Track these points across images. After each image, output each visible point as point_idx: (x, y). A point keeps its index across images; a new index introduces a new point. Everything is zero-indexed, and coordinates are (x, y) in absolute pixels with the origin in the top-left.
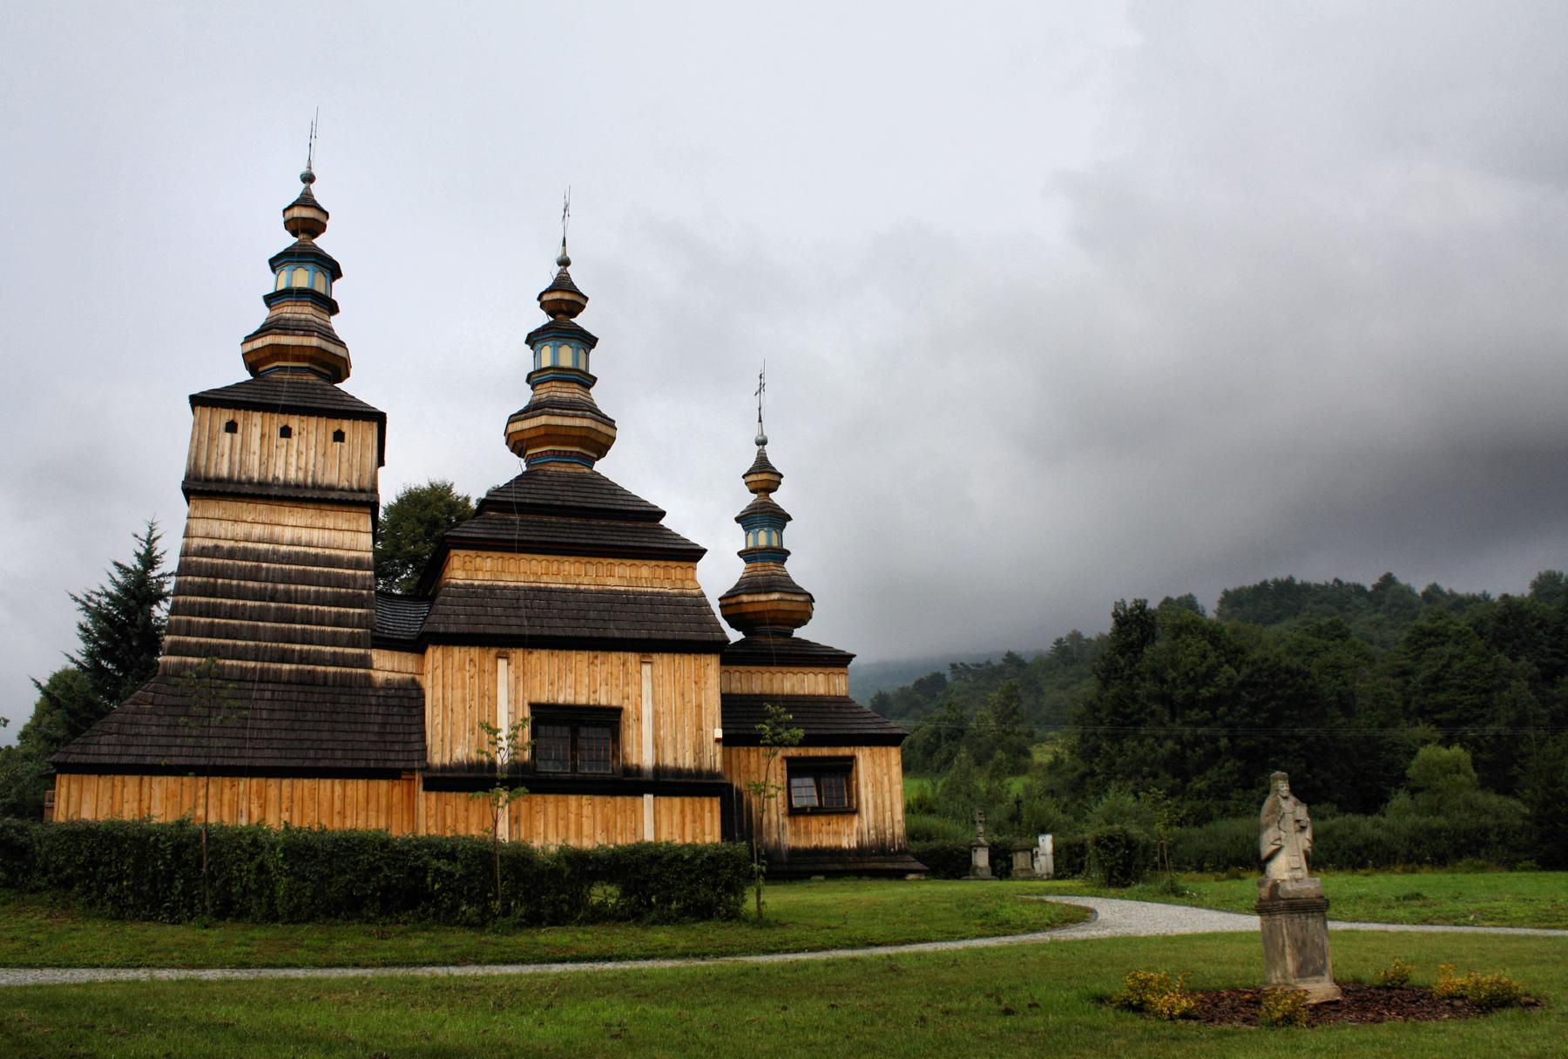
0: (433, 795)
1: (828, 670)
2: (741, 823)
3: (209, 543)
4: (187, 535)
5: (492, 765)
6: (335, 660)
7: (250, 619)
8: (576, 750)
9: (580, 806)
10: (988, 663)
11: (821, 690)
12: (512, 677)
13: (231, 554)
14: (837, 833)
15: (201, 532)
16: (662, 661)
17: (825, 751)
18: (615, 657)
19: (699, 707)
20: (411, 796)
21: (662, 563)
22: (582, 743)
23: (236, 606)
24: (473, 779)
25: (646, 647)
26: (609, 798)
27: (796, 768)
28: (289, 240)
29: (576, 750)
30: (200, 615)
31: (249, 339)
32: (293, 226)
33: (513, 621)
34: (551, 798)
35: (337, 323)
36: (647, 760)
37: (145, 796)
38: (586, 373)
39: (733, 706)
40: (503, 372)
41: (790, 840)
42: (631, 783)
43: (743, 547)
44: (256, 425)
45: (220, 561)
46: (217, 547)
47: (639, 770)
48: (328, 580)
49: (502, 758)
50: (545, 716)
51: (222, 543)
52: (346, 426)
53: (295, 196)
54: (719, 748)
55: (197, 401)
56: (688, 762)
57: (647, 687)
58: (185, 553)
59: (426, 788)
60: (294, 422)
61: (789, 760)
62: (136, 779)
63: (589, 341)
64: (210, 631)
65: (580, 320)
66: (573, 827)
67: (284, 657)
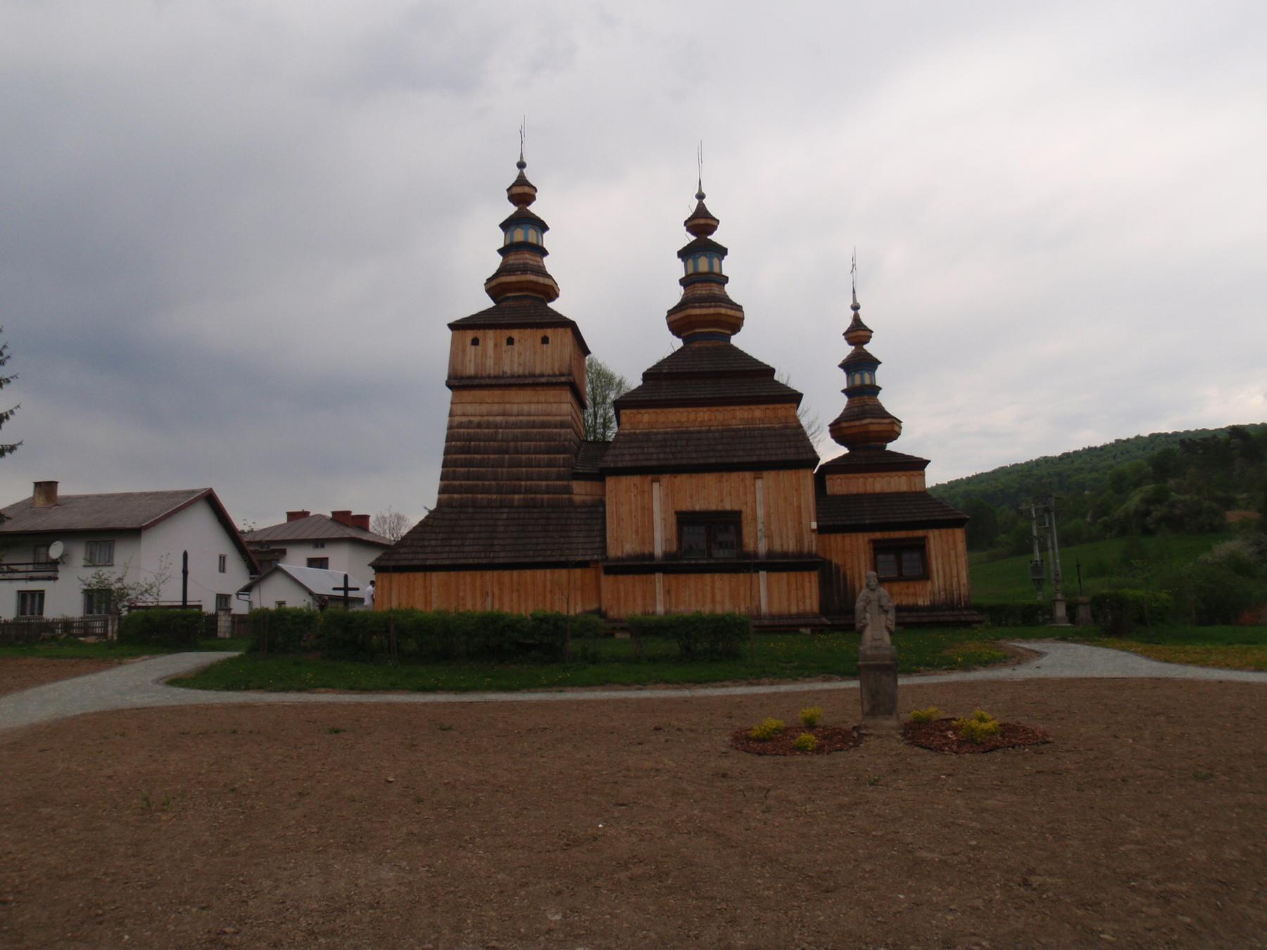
0: (611, 578)
1: (909, 473)
3: (464, 419)
4: (451, 415)
5: (652, 556)
8: (711, 542)
9: (713, 582)
11: (904, 488)
13: (479, 426)
15: (459, 412)
16: (769, 476)
17: (903, 534)
18: (735, 476)
19: (799, 507)
21: (771, 406)
24: (641, 566)
25: (758, 467)
26: (734, 575)
27: (879, 548)
29: (711, 542)
32: (513, 198)
33: (662, 456)
34: (693, 576)
35: (547, 261)
36: (762, 548)
38: (720, 275)
42: (747, 564)
43: (845, 387)
44: (490, 338)
46: (470, 422)
47: (755, 555)
49: (658, 551)
50: (685, 520)
51: (472, 419)
52: (549, 332)
54: (814, 536)
55: (453, 326)
56: (791, 546)
57: (759, 496)
60: (515, 334)
61: (874, 542)
63: (722, 252)
64: (468, 477)
65: (715, 237)
66: (709, 596)
67: (516, 491)
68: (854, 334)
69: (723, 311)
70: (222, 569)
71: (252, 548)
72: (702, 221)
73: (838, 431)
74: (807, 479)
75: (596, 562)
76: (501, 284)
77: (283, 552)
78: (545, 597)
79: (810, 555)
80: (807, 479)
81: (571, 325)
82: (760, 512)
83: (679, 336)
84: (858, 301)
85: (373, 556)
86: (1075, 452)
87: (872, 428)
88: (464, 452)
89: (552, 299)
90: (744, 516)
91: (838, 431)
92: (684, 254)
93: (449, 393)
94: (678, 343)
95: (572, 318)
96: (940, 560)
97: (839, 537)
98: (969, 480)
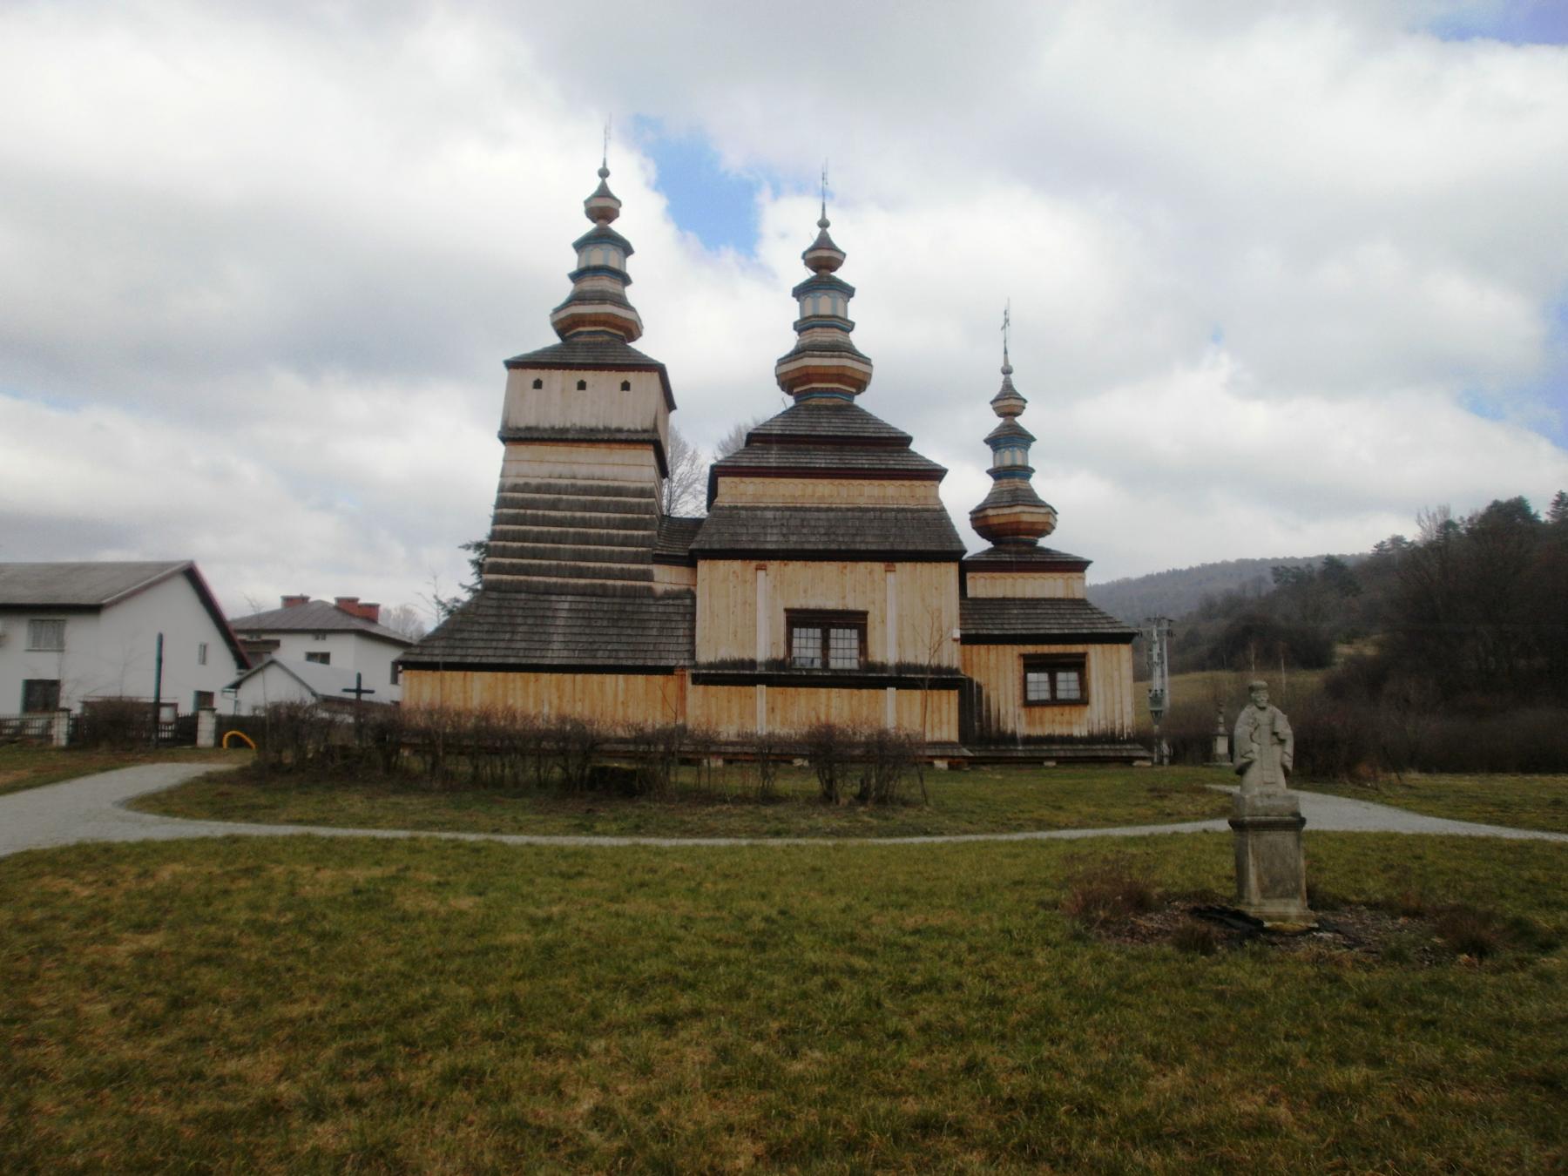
0: (701, 688)
3: (521, 481)
4: (502, 476)
6: (623, 575)
9: (829, 698)
10: (1309, 565)
11: (1060, 594)
13: (538, 489)
14: (1070, 723)
16: (904, 569)
18: (862, 567)
20: (682, 689)
21: (907, 483)
22: (833, 643)
24: (737, 675)
25: (890, 557)
27: (1031, 664)
31: (557, 311)
34: (803, 690)
39: (970, 607)
40: (773, 327)
41: (1023, 730)
42: (871, 677)
43: (991, 466)
44: (558, 381)
48: (618, 508)
50: (797, 619)
52: (631, 377)
54: (957, 646)
55: (512, 365)
57: (891, 593)
59: (694, 683)
60: (588, 376)
63: (848, 292)
64: (522, 553)
65: (839, 274)
68: (1006, 403)
70: (203, 661)
72: (825, 253)
73: (980, 521)
74: (953, 569)
75: (683, 668)
76: (573, 316)
77: (277, 644)
79: (950, 670)
81: (660, 370)
82: (891, 614)
83: (790, 392)
85: (396, 654)
86: (1159, 575)
87: (1026, 518)
89: (633, 339)
90: (870, 618)
92: (800, 292)
93: (500, 449)
94: (790, 401)
97: (983, 649)
98: (1191, 572)
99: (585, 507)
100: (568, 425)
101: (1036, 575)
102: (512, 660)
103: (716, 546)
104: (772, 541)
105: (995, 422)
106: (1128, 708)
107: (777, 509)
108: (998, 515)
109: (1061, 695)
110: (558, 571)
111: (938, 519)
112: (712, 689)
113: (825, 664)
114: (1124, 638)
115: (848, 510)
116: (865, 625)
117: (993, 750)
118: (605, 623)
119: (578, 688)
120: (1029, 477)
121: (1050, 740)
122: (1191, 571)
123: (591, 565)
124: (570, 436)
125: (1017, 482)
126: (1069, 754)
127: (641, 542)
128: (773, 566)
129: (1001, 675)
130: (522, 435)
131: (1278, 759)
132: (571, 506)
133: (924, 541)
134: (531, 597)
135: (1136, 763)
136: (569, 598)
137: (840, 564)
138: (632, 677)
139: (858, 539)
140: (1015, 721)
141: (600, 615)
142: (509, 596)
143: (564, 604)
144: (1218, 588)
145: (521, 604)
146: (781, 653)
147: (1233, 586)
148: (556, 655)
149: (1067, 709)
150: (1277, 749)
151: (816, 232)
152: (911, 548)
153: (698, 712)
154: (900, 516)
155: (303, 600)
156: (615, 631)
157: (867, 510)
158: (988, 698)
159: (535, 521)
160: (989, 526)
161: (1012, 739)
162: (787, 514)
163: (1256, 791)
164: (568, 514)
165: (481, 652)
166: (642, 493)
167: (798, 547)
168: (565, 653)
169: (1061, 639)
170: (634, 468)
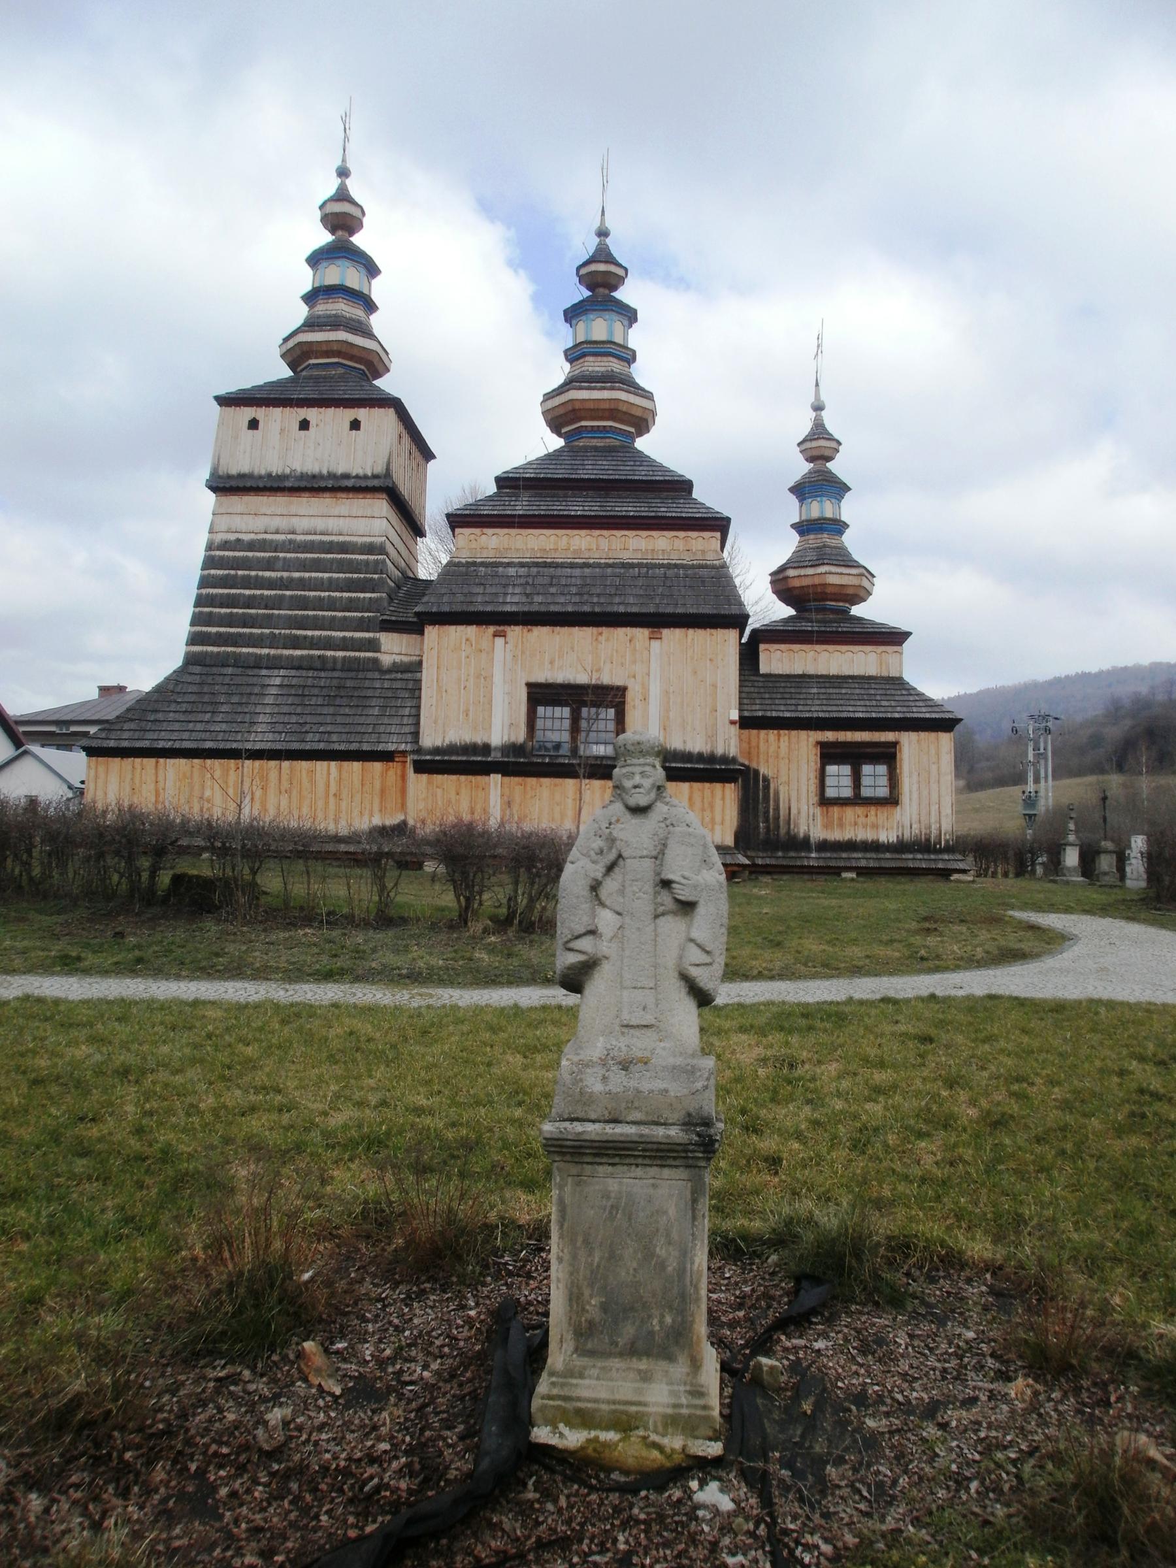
0: (425, 777)
2: (767, 812)
3: (232, 537)
6: (345, 645)
7: (266, 608)
11: (872, 671)
12: (509, 657)
14: (875, 826)
15: (224, 528)
16: (672, 636)
18: (621, 633)
20: (403, 777)
21: (682, 534)
23: (254, 596)
24: (468, 761)
25: (656, 622)
27: (829, 754)
28: (326, 238)
30: (221, 606)
34: (546, 781)
37: (161, 778)
41: (818, 833)
44: (275, 419)
45: (241, 554)
46: (238, 540)
48: (342, 566)
50: (541, 695)
51: (241, 536)
52: (362, 414)
53: (331, 191)
54: (734, 730)
55: (225, 401)
57: (655, 666)
58: (210, 547)
60: (311, 414)
61: (823, 745)
62: (153, 760)
64: (230, 621)
69: (623, 396)
71: (22, 729)
72: (602, 267)
74: (728, 643)
75: (404, 753)
76: (300, 343)
78: (327, 803)
79: (725, 759)
80: (728, 643)
81: (397, 405)
82: (655, 690)
83: (560, 435)
84: (823, 397)
86: (1067, 677)
87: (832, 580)
88: (232, 586)
89: (378, 375)
90: (629, 696)
91: (782, 585)
93: (212, 496)
95: (396, 395)
96: (915, 778)
97: (772, 734)
99: (304, 566)
100: (288, 471)
101: (844, 648)
102: (208, 745)
103: (446, 609)
104: (513, 602)
105: (801, 468)
106: (947, 810)
107: (522, 565)
108: (802, 577)
109: (866, 792)
110: (273, 642)
111: (719, 579)
112: (439, 778)
113: (574, 751)
114: (945, 724)
115: (608, 566)
116: (624, 703)
117: (779, 858)
118: (320, 701)
119: (285, 777)
120: (840, 532)
121: (851, 846)
122: (1100, 674)
123: (309, 633)
124: (288, 484)
125: (825, 538)
126: (872, 864)
127: (369, 606)
128: (515, 632)
129: (792, 766)
130: (234, 483)
131: (669, 960)
132: (288, 566)
133: (707, 606)
134: (239, 671)
135: (955, 877)
136: (282, 673)
137: (595, 630)
138: (346, 764)
139: (617, 600)
140: (809, 822)
141: (316, 691)
142: (215, 670)
143: (276, 679)
144: (1125, 691)
145: (227, 680)
146: (520, 736)
147: (1144, 689)
148: (261, 739)
149: (873, 810)
150: (673, 927)
151: (593, 242)
152: (680, 610)
153: (421, 806)
154: (670, 573)
155: (121, 689)
156: (331, 710)
157: (632, 566)
158: (777, 793)
159: (247, 583)
160: (790, 590)
161: (804, 844)
162: (534, 570)
163: (596, 1049)
164: (285, 574)
165: (175, 736)
166: (370, 549)
167: (543, 609)
168: (270, 736)
169: (869, 729)
170: (369, 520)
